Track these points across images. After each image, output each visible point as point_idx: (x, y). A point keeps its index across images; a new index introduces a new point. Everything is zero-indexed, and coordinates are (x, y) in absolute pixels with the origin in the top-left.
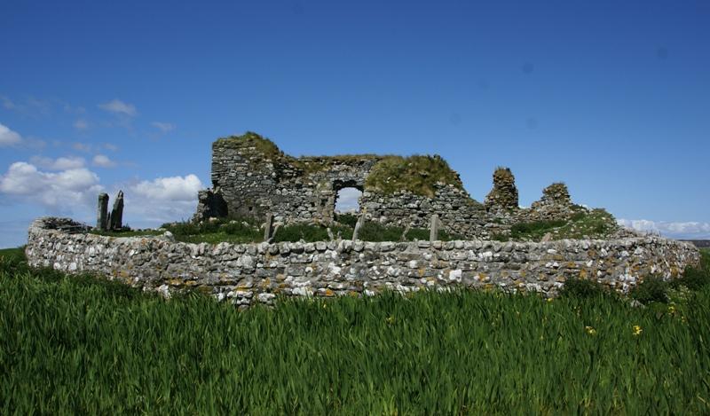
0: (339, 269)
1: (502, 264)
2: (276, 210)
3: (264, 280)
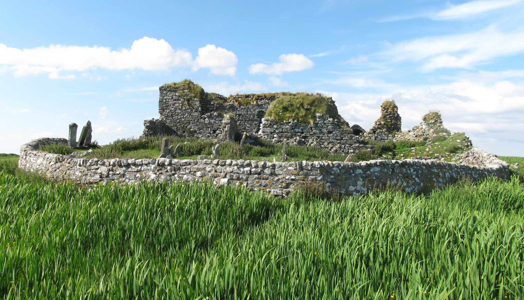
0: (155, 175)
1: (257, 176)
2: (200, 133)
3: (113, 181)
